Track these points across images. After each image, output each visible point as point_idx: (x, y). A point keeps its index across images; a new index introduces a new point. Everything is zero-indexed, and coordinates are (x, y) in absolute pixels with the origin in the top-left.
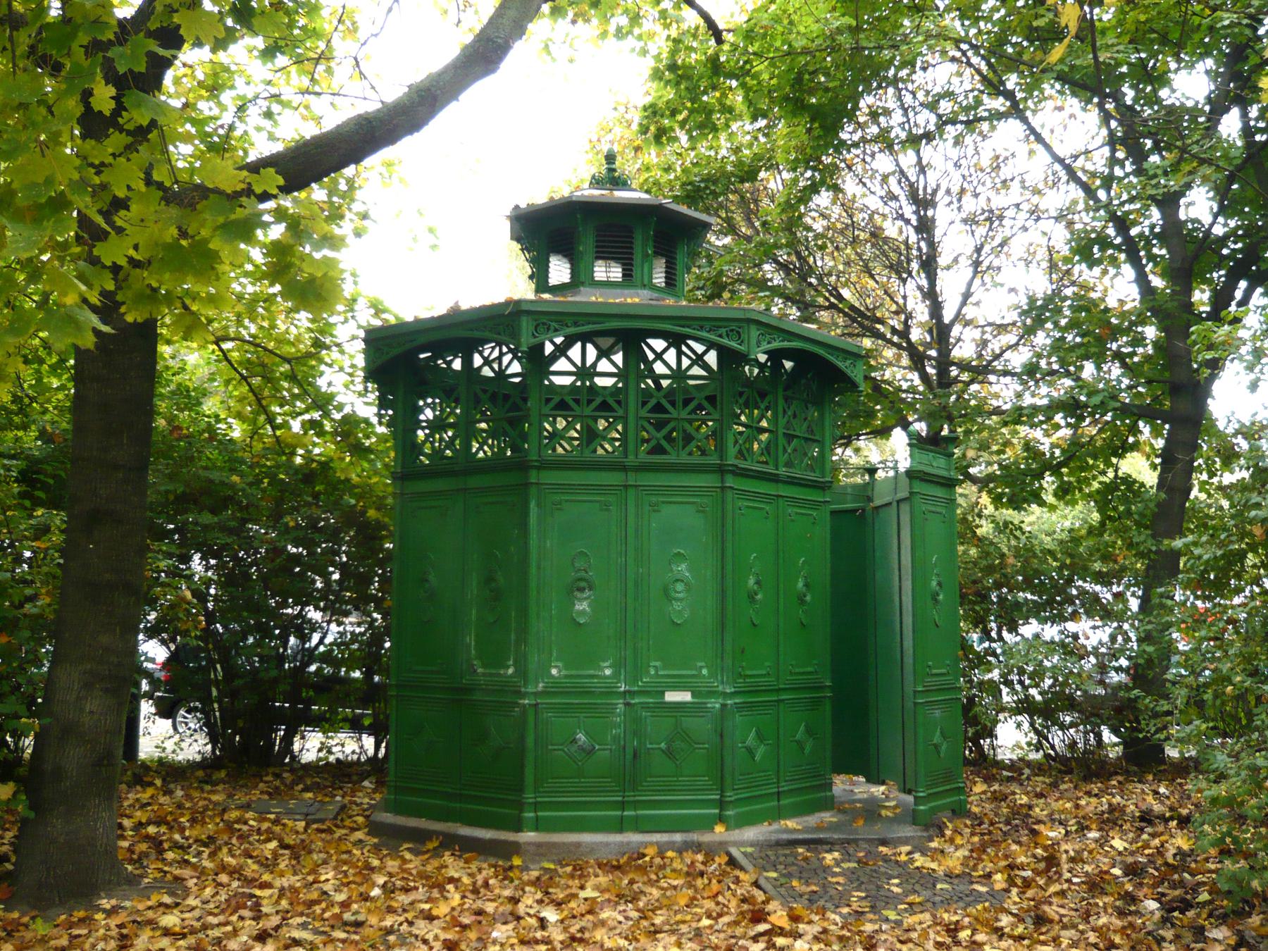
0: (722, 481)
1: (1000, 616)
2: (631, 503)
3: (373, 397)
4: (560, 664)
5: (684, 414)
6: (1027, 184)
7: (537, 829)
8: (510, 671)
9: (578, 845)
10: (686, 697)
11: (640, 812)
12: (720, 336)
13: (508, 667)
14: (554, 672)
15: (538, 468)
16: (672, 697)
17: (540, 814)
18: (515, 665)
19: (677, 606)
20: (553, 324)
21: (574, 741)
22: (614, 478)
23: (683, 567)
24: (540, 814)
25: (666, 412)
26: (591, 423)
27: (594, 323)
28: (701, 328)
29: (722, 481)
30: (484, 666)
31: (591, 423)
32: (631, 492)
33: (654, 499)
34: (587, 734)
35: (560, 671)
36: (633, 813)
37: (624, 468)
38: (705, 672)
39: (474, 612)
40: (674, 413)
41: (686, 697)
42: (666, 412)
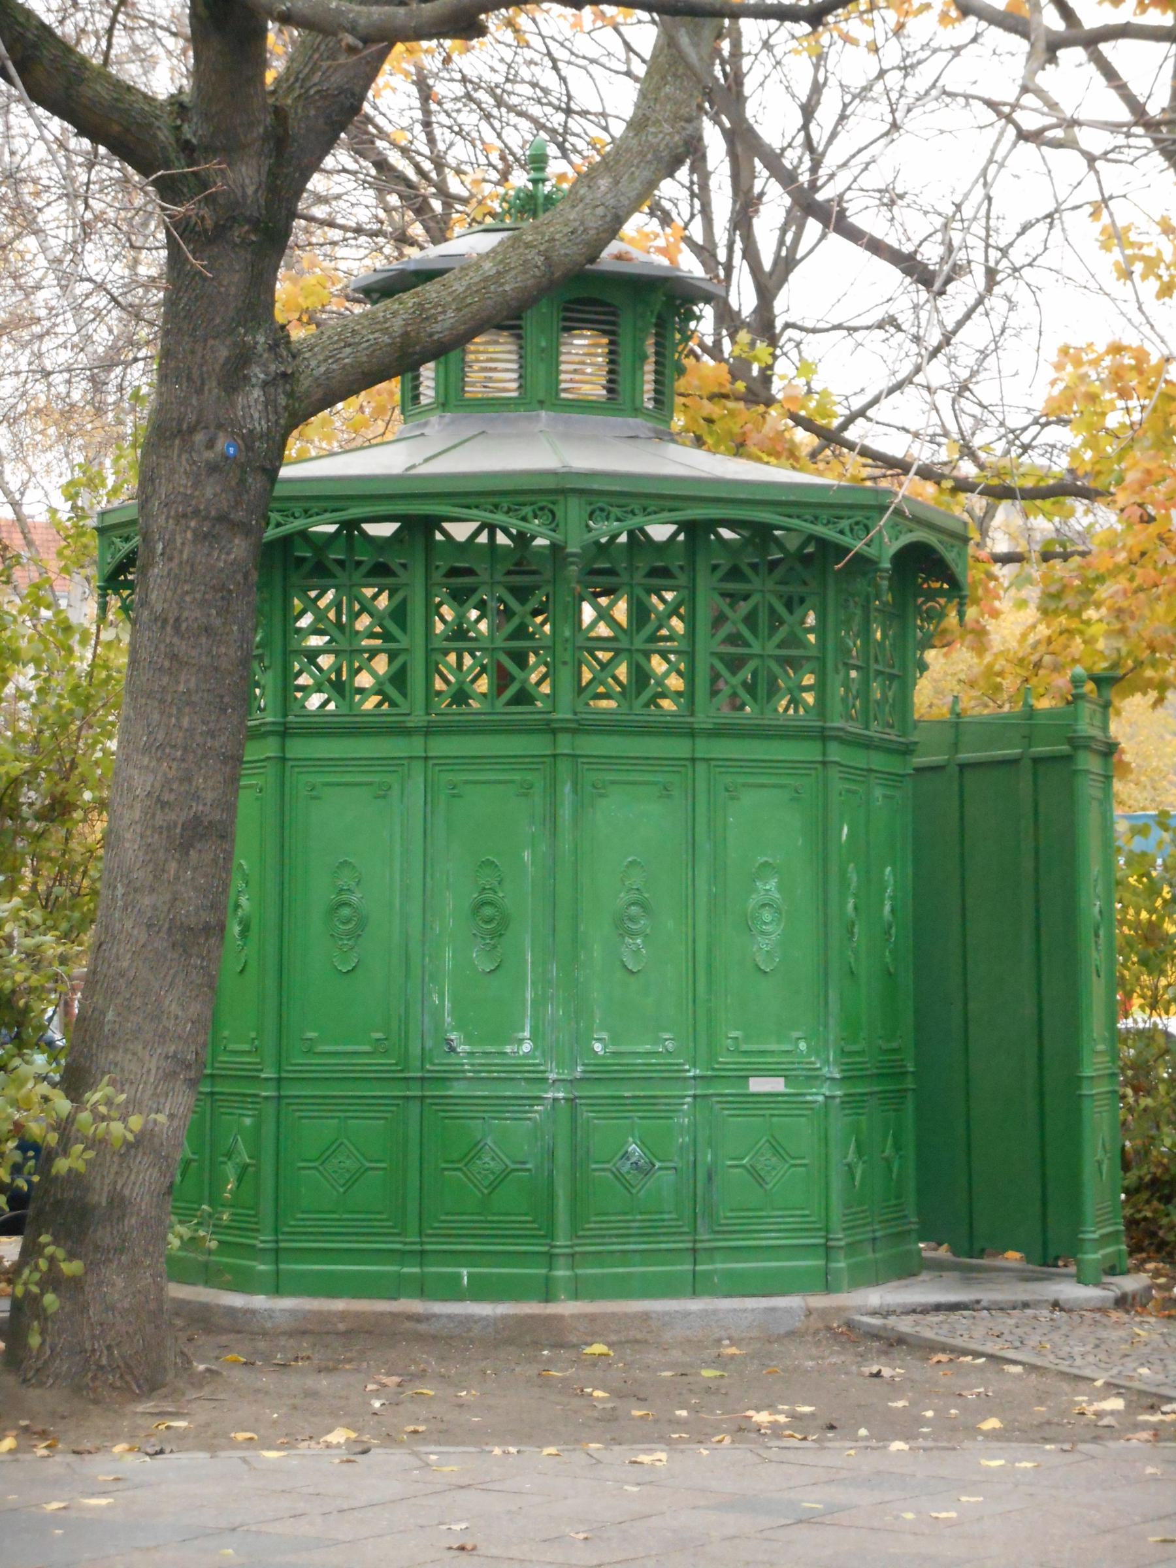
0: (824, 754)
1: (111, 871)
2: (701, 786)
3: (973, 706)
4: (604, 1035)
5: (771, 648)
6: (389, 91)
7: (576, 1296)
8: (526, 1047)
9: (646, 1316)
10: (776, 1085)
11: (405, 1270)
12: (842, 532)
13: (521, 1041)
14: (598, 1047)
15: (574, 731)
16: (757, 1085)
17: (579, 1271)
18: (533, 1038)
19: (764, 944)
20: (616, 511)
21: (626, 1156)
22: (679, 748)
23: (772, 885)
24: (579, 1271)
25: (747, 644)
26: (641, 659)
27: (670, 510)
28: (815, 520)
29: (824, 754)
30: (469, 1040)
31: (641, 659)
32: (701, 768)
33: (728, 779)
34: (643, 1144)
35: (605, 1047)
36: (416, 1270)
37: (692, 733)
38: (803, 1046)
39: (448, 954)
40: (756, 648)
41: (776, 1085)
42: (747, 644)
